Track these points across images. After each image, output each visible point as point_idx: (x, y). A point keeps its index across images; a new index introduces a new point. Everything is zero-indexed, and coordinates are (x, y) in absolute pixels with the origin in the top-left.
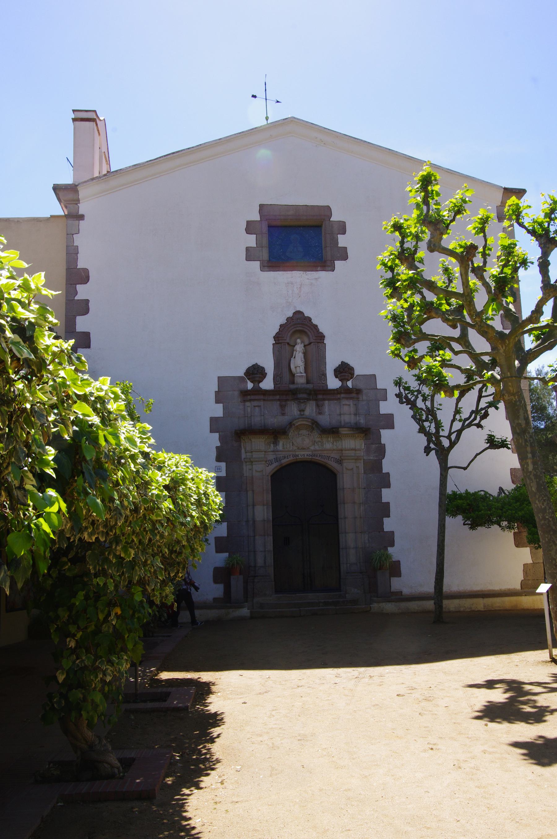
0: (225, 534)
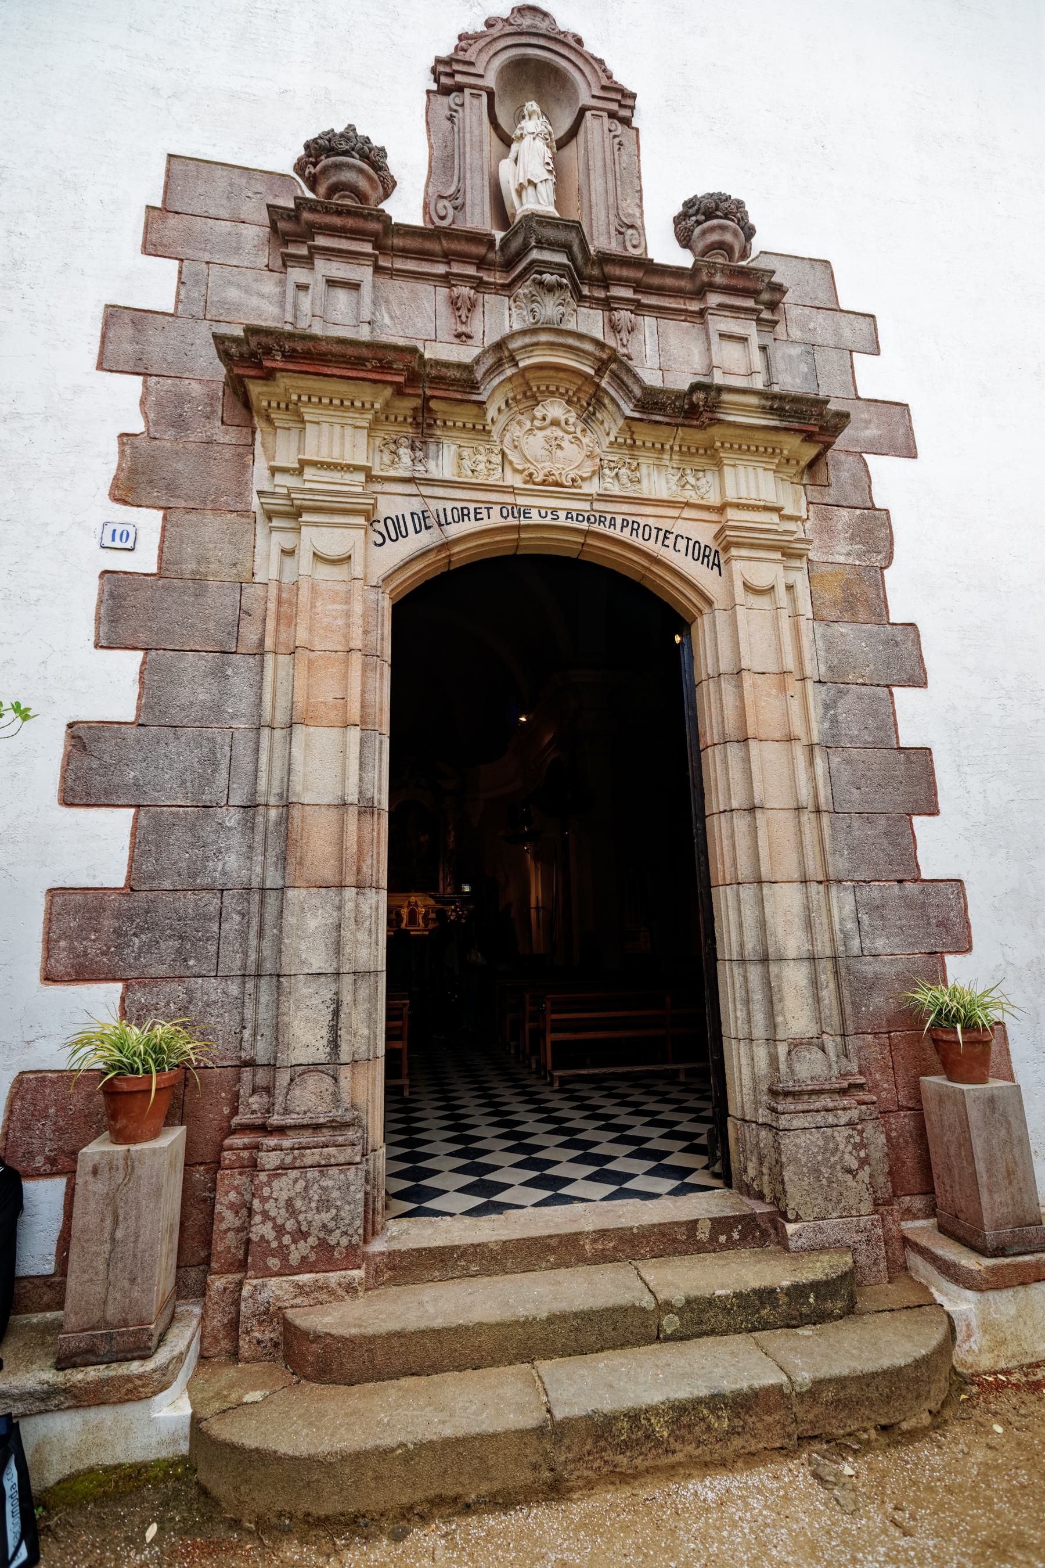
0: (115, 876)
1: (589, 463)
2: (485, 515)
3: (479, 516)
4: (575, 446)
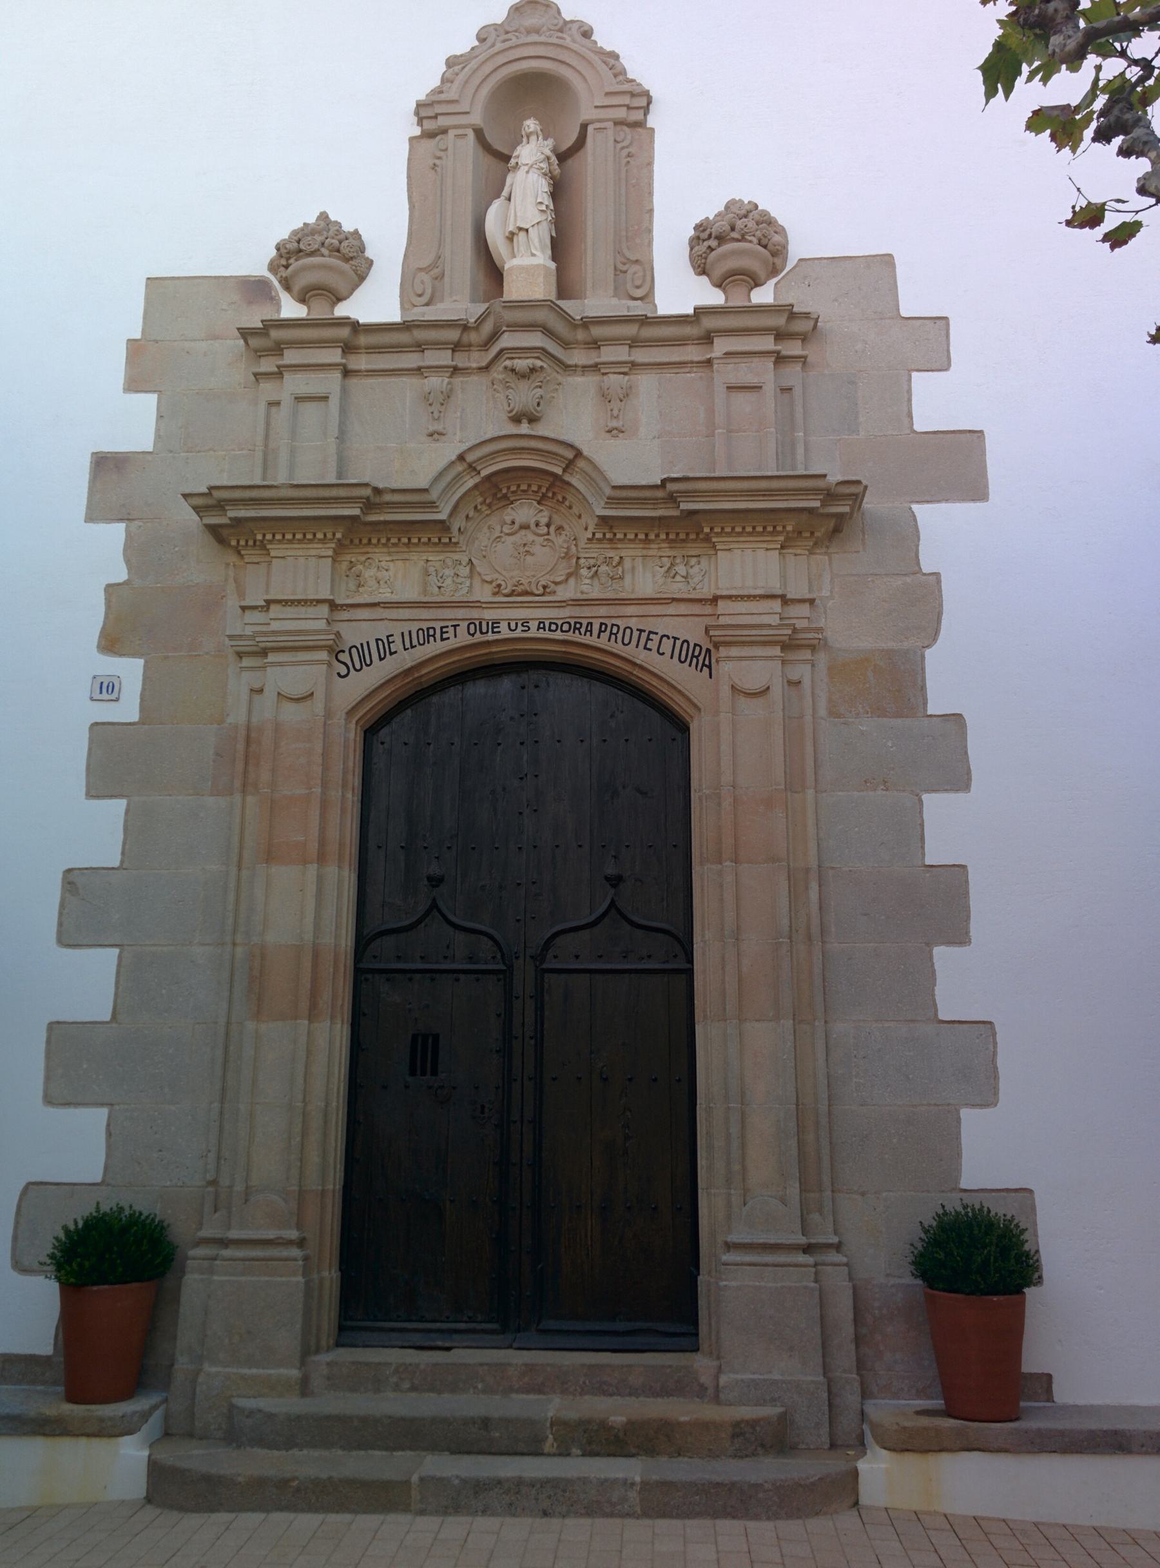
2: (451, 634)
3: (445, 636)
4: (546, 549)
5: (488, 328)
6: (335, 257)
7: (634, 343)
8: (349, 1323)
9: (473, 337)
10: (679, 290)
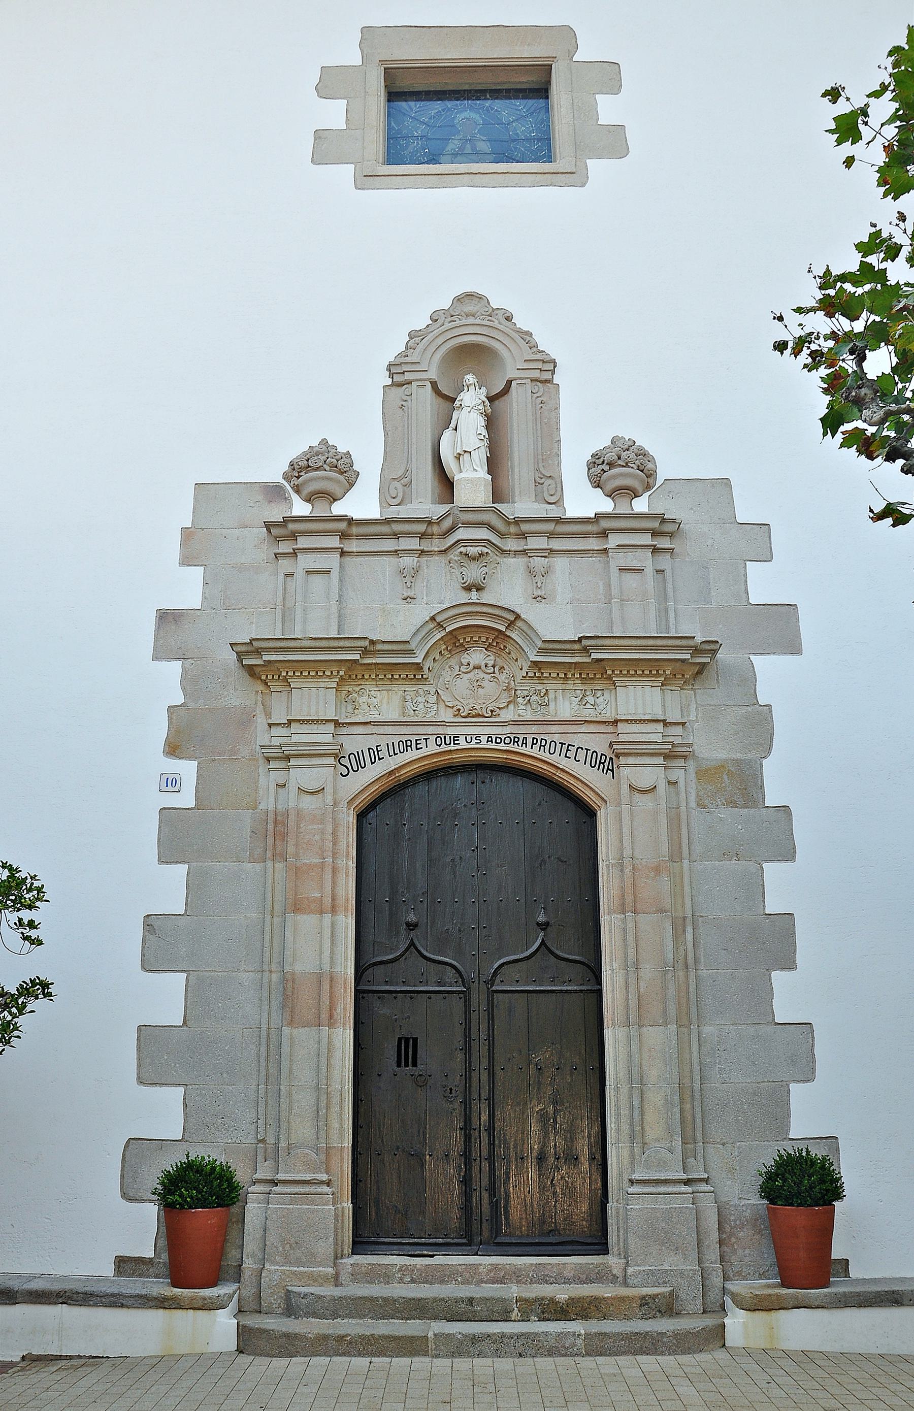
1: (505, 694)
2: (423, 745)
3: (419, 746)
5: (447, 524)
6: (335, 472)
7: (551, 535)
8: (359, 1239)
9: (435, 529)
10: (583, 500)
